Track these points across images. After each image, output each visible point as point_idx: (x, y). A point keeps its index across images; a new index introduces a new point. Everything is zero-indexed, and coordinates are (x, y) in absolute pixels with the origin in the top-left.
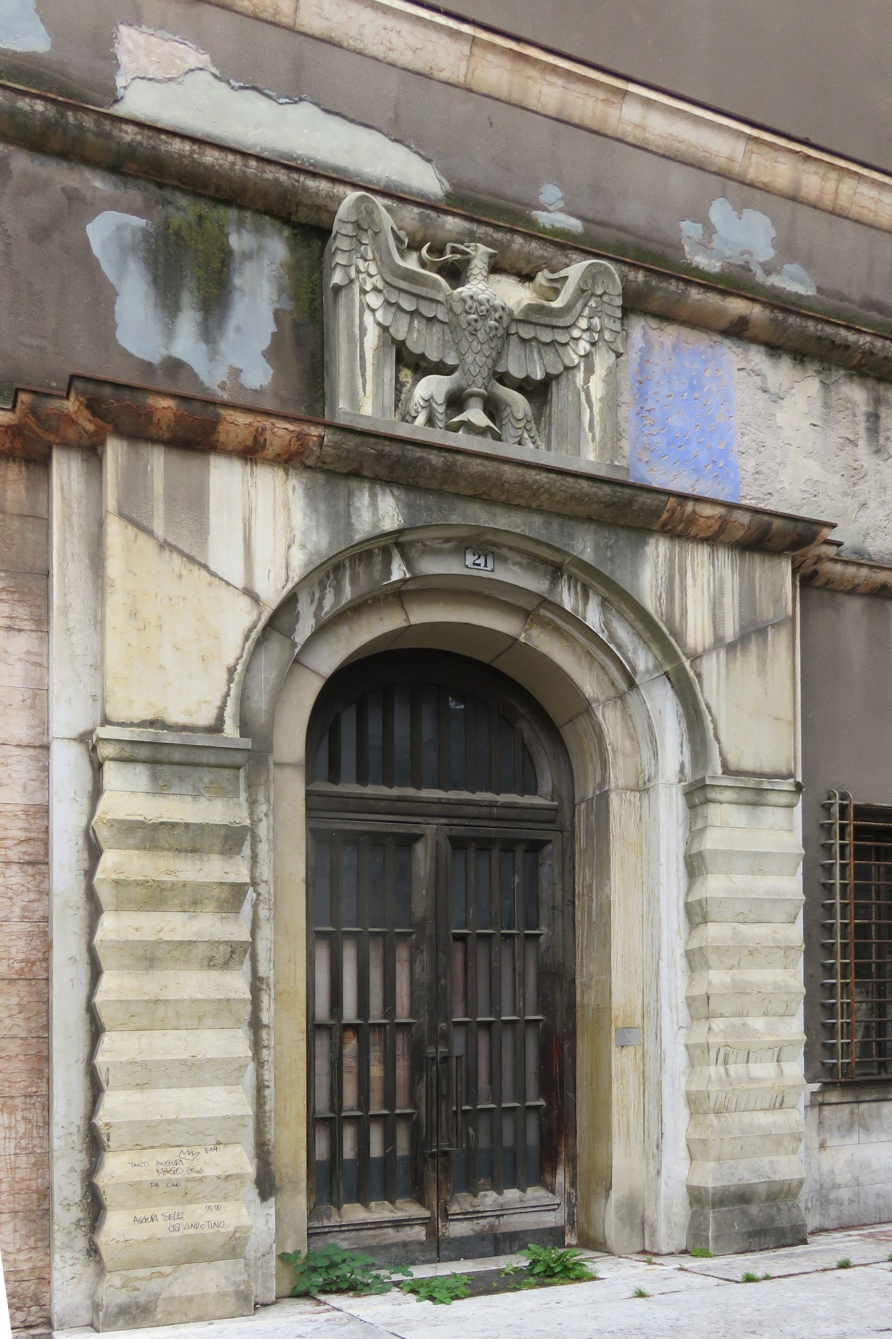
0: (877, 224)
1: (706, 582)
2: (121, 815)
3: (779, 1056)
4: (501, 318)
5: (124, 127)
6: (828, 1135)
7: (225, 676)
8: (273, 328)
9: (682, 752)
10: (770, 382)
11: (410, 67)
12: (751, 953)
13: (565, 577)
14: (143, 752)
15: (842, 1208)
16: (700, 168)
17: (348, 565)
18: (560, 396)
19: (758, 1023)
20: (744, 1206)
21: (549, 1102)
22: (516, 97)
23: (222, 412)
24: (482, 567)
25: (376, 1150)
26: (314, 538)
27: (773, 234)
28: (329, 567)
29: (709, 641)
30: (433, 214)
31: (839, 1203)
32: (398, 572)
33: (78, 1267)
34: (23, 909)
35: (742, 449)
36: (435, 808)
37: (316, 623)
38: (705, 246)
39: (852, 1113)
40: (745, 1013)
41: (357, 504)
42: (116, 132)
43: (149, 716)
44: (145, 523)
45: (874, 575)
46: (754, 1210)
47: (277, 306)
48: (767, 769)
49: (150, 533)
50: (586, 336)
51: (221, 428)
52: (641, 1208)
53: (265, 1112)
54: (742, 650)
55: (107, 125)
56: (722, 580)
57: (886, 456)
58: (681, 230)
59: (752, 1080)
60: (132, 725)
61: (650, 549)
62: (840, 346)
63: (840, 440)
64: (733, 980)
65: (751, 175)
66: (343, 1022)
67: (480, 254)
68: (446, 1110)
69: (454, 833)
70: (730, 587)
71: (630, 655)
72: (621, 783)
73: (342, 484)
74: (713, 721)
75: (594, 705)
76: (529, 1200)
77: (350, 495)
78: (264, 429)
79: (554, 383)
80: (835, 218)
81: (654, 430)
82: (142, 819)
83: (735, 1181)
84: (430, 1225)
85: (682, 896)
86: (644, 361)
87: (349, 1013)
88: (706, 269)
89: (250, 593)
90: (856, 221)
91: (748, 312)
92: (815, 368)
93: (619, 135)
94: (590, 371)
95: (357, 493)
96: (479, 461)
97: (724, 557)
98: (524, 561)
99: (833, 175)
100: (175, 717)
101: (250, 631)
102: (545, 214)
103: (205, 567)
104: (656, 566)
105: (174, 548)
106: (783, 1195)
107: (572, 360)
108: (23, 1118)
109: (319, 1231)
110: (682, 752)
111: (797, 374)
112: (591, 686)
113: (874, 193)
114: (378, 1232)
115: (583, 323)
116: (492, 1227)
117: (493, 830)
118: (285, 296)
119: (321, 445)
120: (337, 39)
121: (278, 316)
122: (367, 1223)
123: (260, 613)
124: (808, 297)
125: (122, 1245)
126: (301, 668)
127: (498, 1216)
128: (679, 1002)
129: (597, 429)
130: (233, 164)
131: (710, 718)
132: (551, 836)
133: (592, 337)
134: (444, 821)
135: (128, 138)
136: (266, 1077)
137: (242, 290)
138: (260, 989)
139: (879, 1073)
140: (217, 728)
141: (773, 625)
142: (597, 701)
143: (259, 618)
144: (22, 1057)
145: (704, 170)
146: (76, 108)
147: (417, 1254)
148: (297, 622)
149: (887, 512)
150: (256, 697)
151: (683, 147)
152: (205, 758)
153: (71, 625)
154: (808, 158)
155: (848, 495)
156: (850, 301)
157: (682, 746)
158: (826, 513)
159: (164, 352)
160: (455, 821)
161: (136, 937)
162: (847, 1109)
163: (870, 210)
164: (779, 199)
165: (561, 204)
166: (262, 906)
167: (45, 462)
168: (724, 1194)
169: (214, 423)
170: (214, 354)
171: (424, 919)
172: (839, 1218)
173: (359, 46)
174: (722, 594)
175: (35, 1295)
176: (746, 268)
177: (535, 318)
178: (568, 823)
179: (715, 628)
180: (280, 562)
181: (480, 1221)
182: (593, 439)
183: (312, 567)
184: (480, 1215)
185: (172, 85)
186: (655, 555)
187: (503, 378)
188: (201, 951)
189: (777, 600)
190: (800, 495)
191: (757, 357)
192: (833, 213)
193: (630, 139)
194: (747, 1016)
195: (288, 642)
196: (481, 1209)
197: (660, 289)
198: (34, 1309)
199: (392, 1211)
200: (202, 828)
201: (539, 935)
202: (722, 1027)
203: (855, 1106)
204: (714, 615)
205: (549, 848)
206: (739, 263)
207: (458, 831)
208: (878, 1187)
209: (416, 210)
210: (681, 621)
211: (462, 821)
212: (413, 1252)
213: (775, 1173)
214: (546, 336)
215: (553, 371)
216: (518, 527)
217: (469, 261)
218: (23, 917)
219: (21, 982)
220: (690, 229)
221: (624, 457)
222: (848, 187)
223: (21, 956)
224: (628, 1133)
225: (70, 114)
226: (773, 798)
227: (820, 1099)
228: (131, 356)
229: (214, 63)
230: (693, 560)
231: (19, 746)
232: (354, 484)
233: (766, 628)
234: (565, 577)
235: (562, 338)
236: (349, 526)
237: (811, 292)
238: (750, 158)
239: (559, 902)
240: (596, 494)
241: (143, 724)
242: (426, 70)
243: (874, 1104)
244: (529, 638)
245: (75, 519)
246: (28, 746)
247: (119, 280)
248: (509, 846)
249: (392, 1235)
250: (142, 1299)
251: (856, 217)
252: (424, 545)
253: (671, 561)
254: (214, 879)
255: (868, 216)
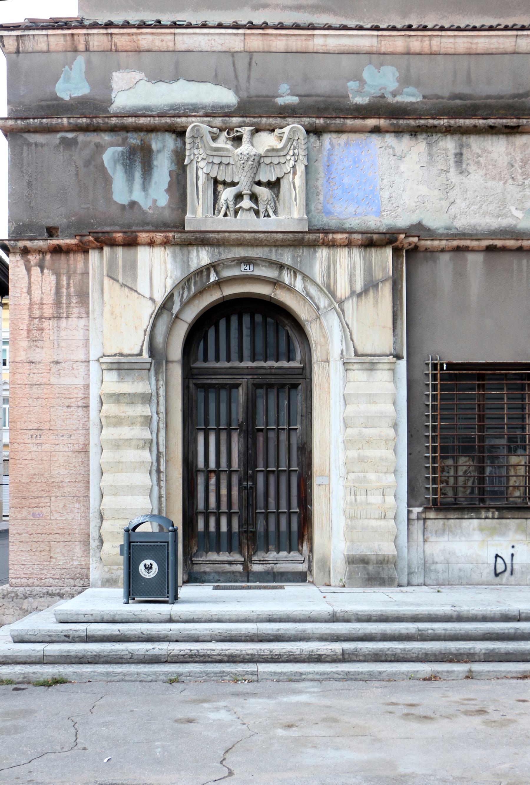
0: (457, 53)
1: (346, 267)
2: (108, 392)
3: (383, 493)
4: (254, 160)
5: (112, 119)
6: (430, 535)
7: (143, 333)
8: (169, 179)
9: (342, 344)
10: (396, 151)
11: (221, 50)
12: (368, 442)
13: (286, 269)
14: (115, 366)
15: (439, 574)
16: (357, 53)
17: (193, 278)
18: (284, 184)
19: (372, 476)
20: (366, 565)
21: (300, 511)
22: (266, 49)
23: (138, 234)
24: (248, 270)
25: (224, 528)
26: (175, 273)
27: (397, 74)
28: (186, 280)
29: (348, 293)
30: (227, 119)
31: (436, 571)
32: (213, 278)
33: (97, 564)
34: (83, 424)
35: (382, 187)
36: (246, 371)
37: (181, 304)
38: (359, 92)
39: (444, 524)
40: (366, 471)
41: (192, 256)
42: (109, 121)
43: (117, 351)
44: (116, 277)
45: (450, 243)
46: (370, 568)
47: (171, 169)
48: (378, 352)
49: (117, 281)
50: (293, 158)
51: (138, 239)
52: (328, 564)
53: (162, 507)
54: (365, 295)
55: (106, 120)
56: (354, 263)
57: (466, 174)
58: (348, 87)
59: (368, 504)
60: (112, 356)
61: (318, 255)
62: (431, 127)
63: (439, 171)
64: (359, 455)
65: (383, 50)
66: (209, 469)
67: (246, 131)
68: (253, 511)
69: (255, 382)
70: (359, 265)
71: (316, 301)
72: (319, 359)
73: (185, 250)
74: (350, 332)
75: (306, 323)
76: (290, 557)
77: (189, 252)
78: (153, 237)
79: (281, 180)
80: (433, 56)
81: (335, 188)
82: (114, 392)
83: (359, 553)
84: (245, 564)
85: (342, 413)
86: (330, 154)
87: (212, 465)
88: (361, 103)
89: (152, 299)
90: (446, 54)
91: (378, 123)
92: (423, 137)
93: (315, 51)
94: (295, 173)
95: (192, 251)
96: (234, 234)
97: (356, 252)
98: (267, 265)
99: (426, 39)
100: (126, 351)
101: (152, 314)
102: (281, 98)
103: (136, 291)
104: (321, 262)
105: (126, 286)
106: (386, 562)
107: (287, 169)
108: (83, 505)
109: (197, 562)
110: (342, 344)
111: (413, 142)
112: (305, 314)
113: (452, 40)
114: (222, 565)
115: (291, 153)
116: (273, 568)
117: (273, 380)
118: (173, 164)
119: (174, 238)
120: (191, 50)
121: (171, 173)
122: (217, 561)
123: (155, 307)
124: (417, 102)
125: (107, 555)
126: (180, 320)
127: (275, 564)
128: (340, 464)
129: (298, 200)
130: (150, 121)
131: (348, 330)
132: (301, 381)
133: (295, 158)
134: (250, 377)
135: (113, 122)
136: (162, 493)
137: (157, 166)
138: (160, 457)
139: (479, 504)
140: (140, 354)
141: (382, 282)
142: (307, 321)
143: (155, 309)
144: (82, 482)
145: (360, 54)
146: (96, 117)
147: (239, 577)
148: (173, 305)
149: (468, 204)
150: (158, 338)
151: (347, 48)
152: (136, 366)
153: (95, 317)
154: (410, 36)
155: (443, 199)
156: (442, 98)
157: (342, 342)
158: (430, 211)
159: (129, 199)
160: (255, 377)
161: (112, 437)
162: (441, 522)
163: (451, 48)
164: (400, 56)
165: (289, 92)
166: (161, 422)
167: (88, 252)
168: (353, 558)
169: (136, 238)
170: (147, 195)
171: (242, 422)
172: (437, 580)
173: (200, 49)
174: (355, 269)
175: (87, 574)
176: (383, 97)
177: (270, 154)
178: (308, 375)
179: (351, 287)
180: (163, 285)
181: (267, 565)
182: (296, 205)
183: (175, 285)
184: (266, 562)
185: (131, 90)
186: (321, 256)
187: (259, 183)
188: (134, 443)
189: (384, 269)
190: (415, 204)
191: (390, 139)
192: (431, 54)
193: (321, 51)
194: (367, 472)
195: (170, 314)
196: (267, 559)
197: (332, 124)
198: (86, 580)
199: (228, 557)
200: (135, 395)
201: (296, 429)
202: (353, 478)
203: (446, 521)
204: (351, 281)
205: (300, 387)
206: (378, 95)
207: (257, 381)
208: (460, 565)
209: (220, 119)
210: (334, 286)
211: (258, 376)
212: (237, 576)
213: (380, 550)
214: (276, 160)
215: (279, 176)
216: (257, 254)
217: (242, 135)
218: (83, 427)
219: (83, 453)
220: (352, 85)
221: (320, 203)
222: (435, 42)
223: (82, 443)
224: (322, 526)
225: (94, 120)
226: (380, 366)
227: (423, 516)
228: (118, 203)
229: (146, 76)
230: (340, 256)
231: (81, 362)
232: (190, 248)
233: (378, 284)
234: (286, 269)
235: (282, 160)
236: (189, 266)
237: (419, 99)
238: (381, 43)
239: (304, 413)
240: (287, 238)
241: (115, 355)
242: (228, 50)
243: (458, 521)
244: (275, 295)
245: (96, 275)
246: (85, 362)
247: (114, 174)
248: (281, 386)
249: (227, 567)
250: (114, 577)
251: (445, 53)
252: (224, 264)
253: (329, 258)
254: (138, 414)
255: (452, 51)
